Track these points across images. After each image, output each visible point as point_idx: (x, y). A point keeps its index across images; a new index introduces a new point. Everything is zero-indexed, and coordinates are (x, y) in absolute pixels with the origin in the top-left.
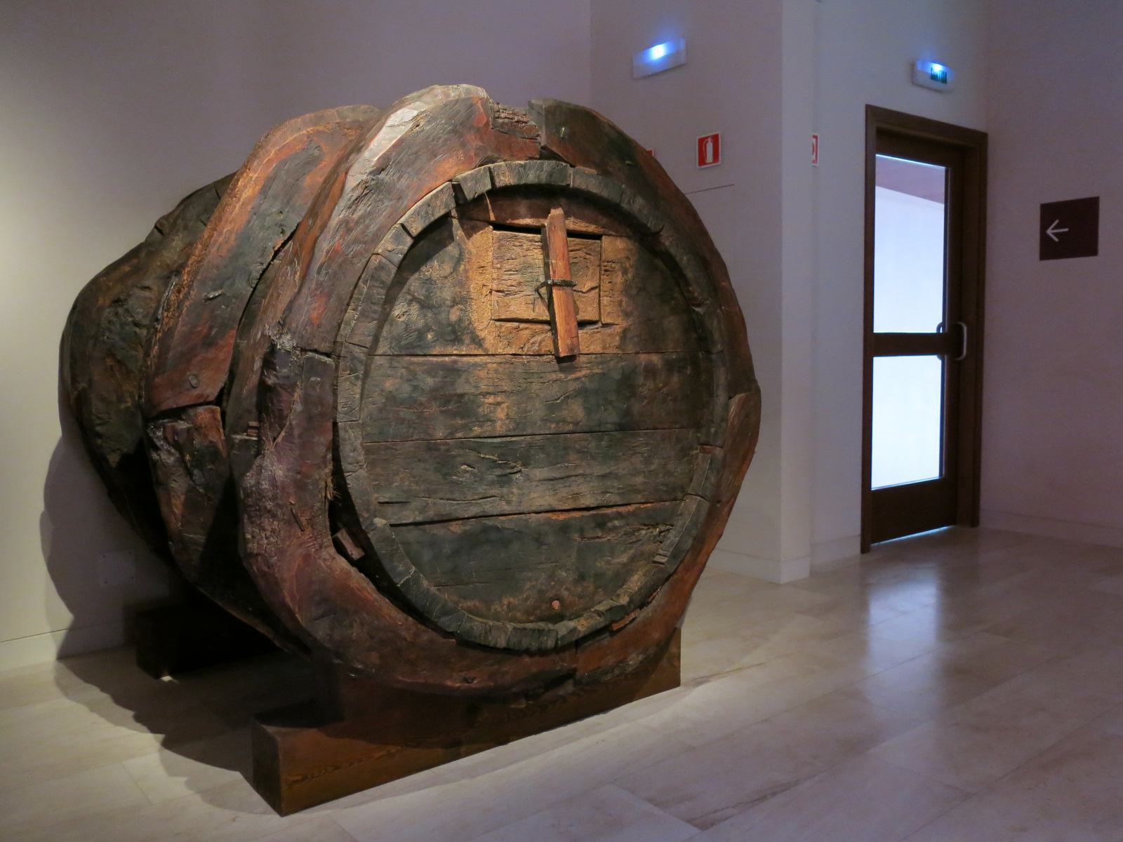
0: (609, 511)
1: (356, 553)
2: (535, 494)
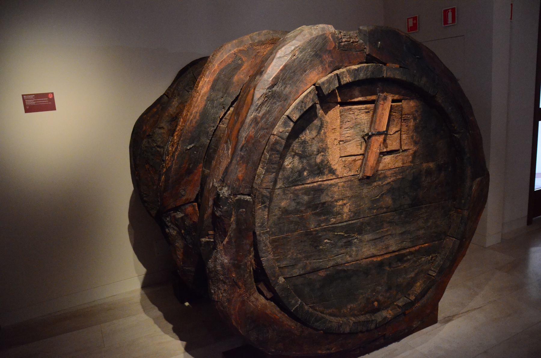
0: (404, 252)
1: (269, 295)
2: (366, 250)
